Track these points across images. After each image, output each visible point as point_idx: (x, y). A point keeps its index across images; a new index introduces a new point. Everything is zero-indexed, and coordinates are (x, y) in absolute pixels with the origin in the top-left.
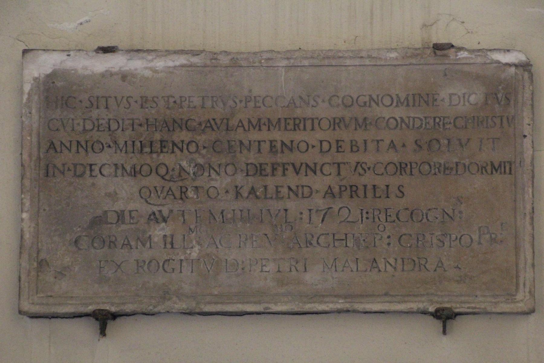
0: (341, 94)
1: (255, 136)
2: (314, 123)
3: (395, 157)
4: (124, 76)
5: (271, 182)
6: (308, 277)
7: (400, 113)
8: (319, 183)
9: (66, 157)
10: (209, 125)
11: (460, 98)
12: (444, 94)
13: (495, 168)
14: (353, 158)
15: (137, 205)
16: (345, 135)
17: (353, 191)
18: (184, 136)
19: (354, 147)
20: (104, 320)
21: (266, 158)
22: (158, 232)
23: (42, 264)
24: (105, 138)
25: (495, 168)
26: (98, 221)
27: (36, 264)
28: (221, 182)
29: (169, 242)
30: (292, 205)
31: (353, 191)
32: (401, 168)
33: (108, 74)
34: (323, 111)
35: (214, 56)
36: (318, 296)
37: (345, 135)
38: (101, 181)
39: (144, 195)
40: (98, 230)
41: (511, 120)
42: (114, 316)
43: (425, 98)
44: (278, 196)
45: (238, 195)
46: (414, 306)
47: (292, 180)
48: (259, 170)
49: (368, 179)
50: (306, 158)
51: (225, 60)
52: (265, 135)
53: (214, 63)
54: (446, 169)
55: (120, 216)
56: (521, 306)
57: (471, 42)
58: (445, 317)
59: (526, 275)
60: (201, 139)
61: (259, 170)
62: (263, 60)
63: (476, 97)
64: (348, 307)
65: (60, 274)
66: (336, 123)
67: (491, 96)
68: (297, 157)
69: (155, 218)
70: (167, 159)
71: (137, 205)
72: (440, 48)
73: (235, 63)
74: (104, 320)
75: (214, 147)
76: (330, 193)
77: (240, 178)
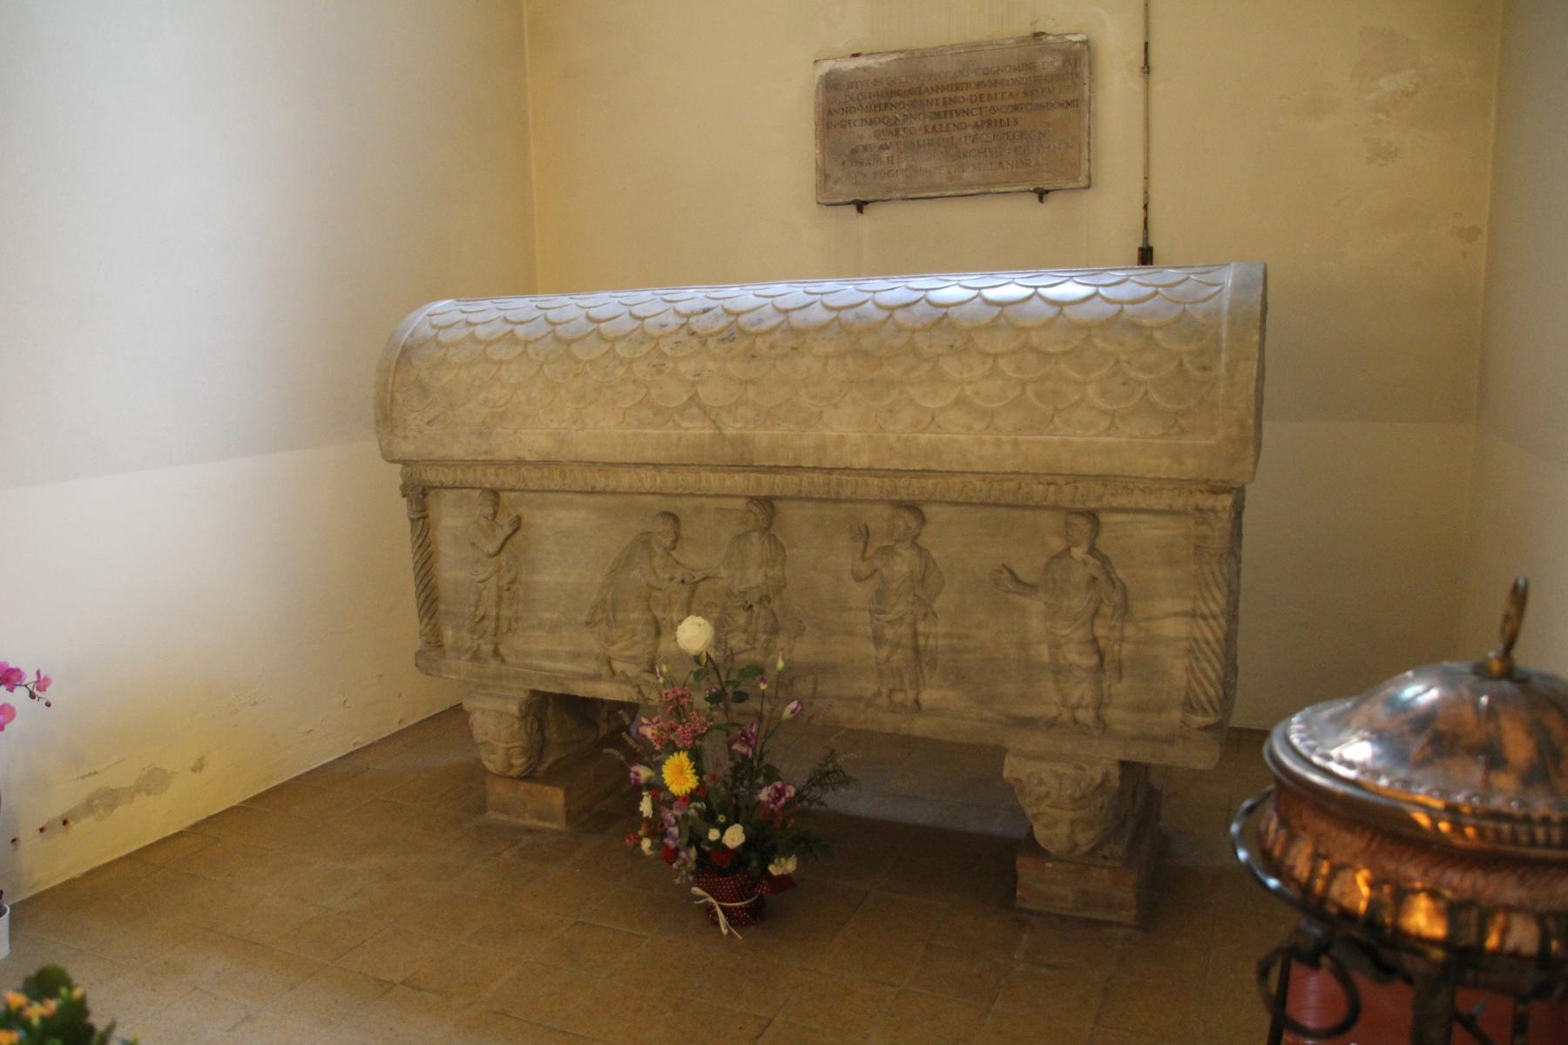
1: (935, 96)
3: (1012, 102)
4: (865, 69)
5: (944, 122)
6: (965, 175)
7: (1014, 75)
8: (970, 120)
9: (836, 118)
10: (911, 92)
11: (1049, 64)
12: (1039, 62)
14: (988, 104)
15: (873, 141)
16: (985, 91)
17: (989, 123)
18: (898, 99)
19: (990, 98)
20: (860, 206)
21: (941, 108)
22: (885, 155)
24: (856, 105)
26: (854, 151)
27: (824, 177)
28: (917, 124)
29: (890, 160)
30: (956, 134)
31: (989, 123)
32: (1016, 108)
33: (857, 69)
34: (973, 78)
35: (912, 52)
36: (970, 185)
37: (985, 91)
38: (854, 129)
39: (877, 135)
41: (1077, 75)
42: (866, 203)
43: (1029, 66)
44: (948, 130)
45: (926, 131)
46: (1022, 188)
47: (956, 120)
48: (938, 115)
49: (997, 116)
50: (963, 106)
51: (917, 54)
52: (940, 95)
53: (913, 57)
54: (1041, 107)
55: (865, 148)
56: (1082, 184)
57: (1058, 31)
58: (1042, 194)
59: (1085, 166)
60: (906, 100)
61: (938, 115)
62: (939, 52)
64: (983, 191)
65: (836, 182)
66: (979, 84)
67: (1066, 61)
68: (958, 106)
69: (883, 147)
70: (888, 113)
71: (873, 141)
72: (1037, 35)
73: (924, 54)
74: (860, 206)
75: (913, 104)
76: (977, 126)
77: (927, 121)
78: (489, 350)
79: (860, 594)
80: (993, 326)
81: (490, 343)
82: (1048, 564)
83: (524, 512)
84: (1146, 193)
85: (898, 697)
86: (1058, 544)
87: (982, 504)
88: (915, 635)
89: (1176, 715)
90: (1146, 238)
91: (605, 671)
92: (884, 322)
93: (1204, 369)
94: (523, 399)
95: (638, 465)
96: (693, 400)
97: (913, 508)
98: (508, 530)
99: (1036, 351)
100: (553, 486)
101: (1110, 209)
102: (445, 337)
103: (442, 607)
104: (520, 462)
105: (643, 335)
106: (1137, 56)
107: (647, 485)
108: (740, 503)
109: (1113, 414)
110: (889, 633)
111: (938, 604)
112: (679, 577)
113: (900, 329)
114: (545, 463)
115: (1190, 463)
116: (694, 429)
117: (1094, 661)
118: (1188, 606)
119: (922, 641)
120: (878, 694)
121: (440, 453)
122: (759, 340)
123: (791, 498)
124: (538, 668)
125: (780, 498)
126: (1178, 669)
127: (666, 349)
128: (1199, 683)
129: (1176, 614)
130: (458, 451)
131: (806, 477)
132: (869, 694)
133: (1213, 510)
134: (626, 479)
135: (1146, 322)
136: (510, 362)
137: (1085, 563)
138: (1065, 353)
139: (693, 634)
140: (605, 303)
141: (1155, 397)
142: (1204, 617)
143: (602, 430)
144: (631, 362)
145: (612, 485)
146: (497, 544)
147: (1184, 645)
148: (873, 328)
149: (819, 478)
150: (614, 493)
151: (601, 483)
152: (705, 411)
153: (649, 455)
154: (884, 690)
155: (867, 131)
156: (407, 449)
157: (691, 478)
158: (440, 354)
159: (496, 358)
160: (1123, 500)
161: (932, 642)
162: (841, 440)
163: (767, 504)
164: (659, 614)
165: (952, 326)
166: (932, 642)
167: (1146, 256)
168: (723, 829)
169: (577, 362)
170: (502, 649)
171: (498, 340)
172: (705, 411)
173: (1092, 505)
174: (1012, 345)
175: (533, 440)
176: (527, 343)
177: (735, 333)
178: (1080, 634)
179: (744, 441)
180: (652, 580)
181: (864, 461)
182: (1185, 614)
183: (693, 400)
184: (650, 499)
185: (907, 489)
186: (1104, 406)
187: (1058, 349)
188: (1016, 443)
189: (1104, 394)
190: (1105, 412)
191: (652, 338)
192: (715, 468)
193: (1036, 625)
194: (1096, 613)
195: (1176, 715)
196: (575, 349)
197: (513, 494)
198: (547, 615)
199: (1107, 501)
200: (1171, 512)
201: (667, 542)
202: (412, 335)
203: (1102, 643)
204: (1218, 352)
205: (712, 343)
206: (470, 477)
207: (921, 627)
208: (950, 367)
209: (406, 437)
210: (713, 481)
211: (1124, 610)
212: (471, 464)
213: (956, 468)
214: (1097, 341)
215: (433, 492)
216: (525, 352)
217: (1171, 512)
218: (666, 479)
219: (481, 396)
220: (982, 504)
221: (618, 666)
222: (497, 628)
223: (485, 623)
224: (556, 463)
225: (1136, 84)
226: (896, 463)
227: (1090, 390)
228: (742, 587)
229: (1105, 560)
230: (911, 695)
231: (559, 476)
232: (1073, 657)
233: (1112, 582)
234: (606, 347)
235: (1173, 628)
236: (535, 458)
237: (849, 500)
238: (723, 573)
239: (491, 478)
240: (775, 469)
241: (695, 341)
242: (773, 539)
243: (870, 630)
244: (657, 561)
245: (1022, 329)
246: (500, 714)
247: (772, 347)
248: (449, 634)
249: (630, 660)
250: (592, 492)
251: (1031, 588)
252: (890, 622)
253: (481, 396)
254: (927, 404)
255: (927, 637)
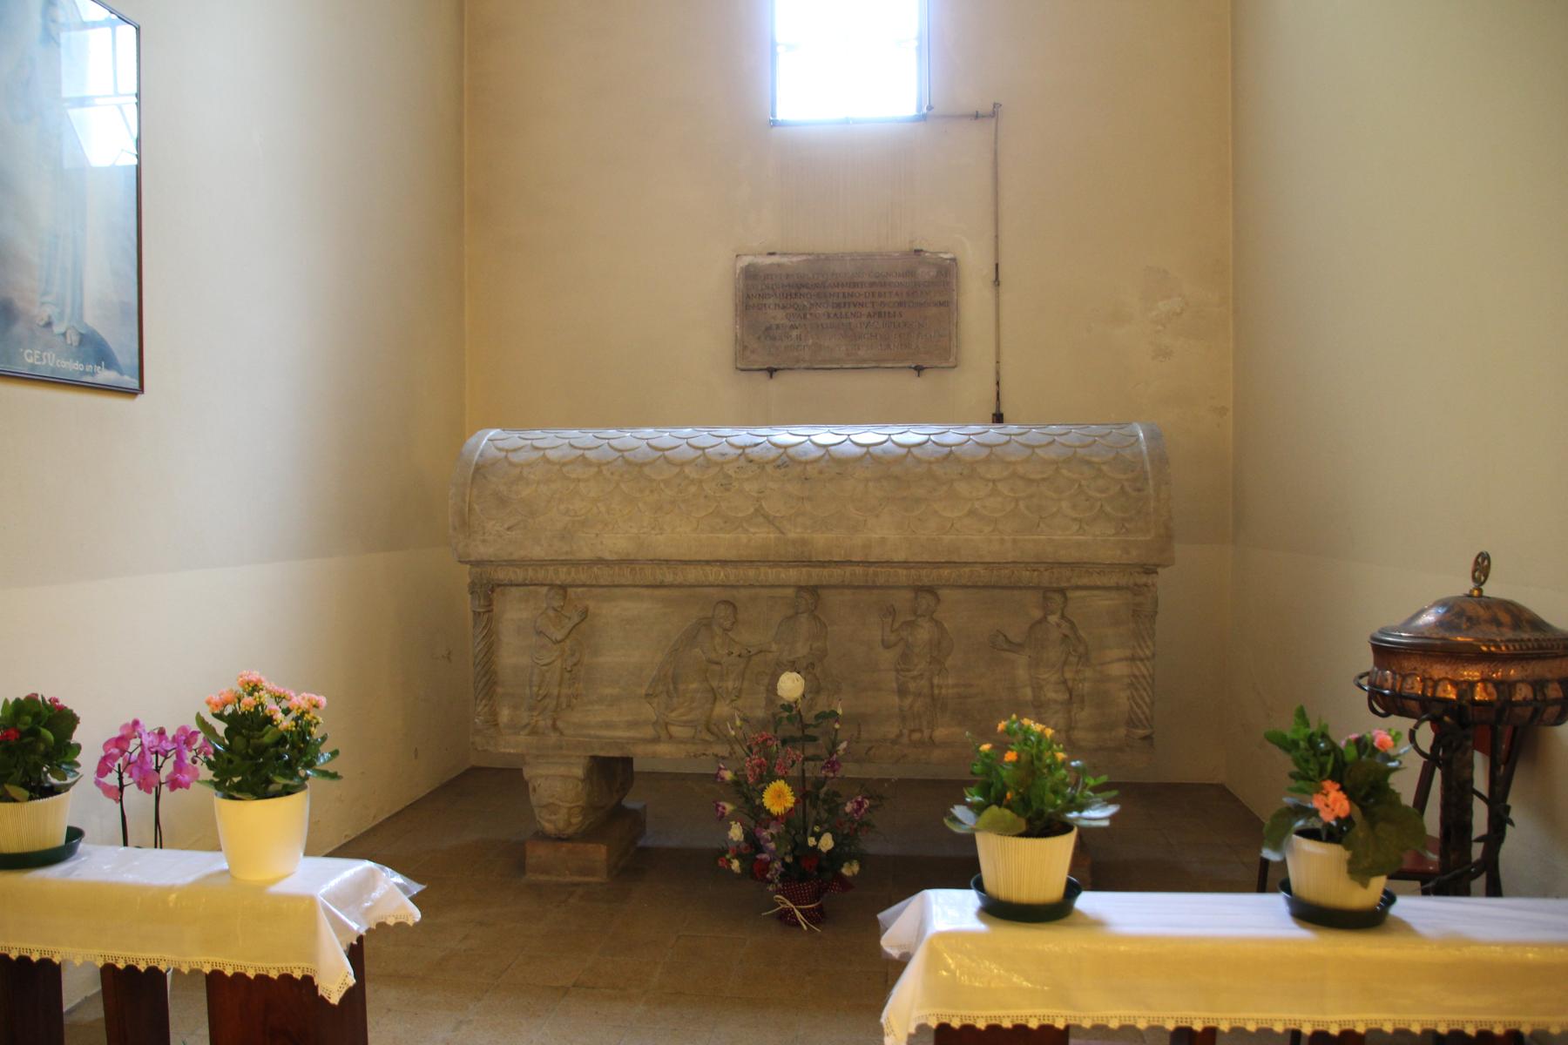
0: (170, 734)
2: (863, 284)
3: (896, 299)
4: (779, 265)
5: (843, 311)
7: (900, 280)
8: (865, 311)
10: (816, 286)
11: (926, 273)
12: (920, 271)
13: (941, 304)
15: (785, 321)
17: (880, 314)
19: (880, 295)
22: (795, 333)
23: (745, 348)
25: (941, 304)
26: (768, 329)
27: (742, 348)
28: (821, 311)
29: (799, 338)
30: (853, 320)
31: (880, 314)
33: (772, 265)
36: (865, 361)
40: (768, 332)
43: (910, 273)
47: (853, 309)
48: (838, 305)
49: (886, 309)
58: (919, 369)
61: (838, 305)
63: (933, 273)
64: (878, 366)
65: (753, 352)
66: (872, 284)
68: (854, 300)
69: (793, 327)
70: (798, 301)
71: (785, 321)
72: (918, 252)
74: (771, 371)
75: (818, 295)
76: (869, 315)
78: (565, 469)
79: (888, 657)
80: (987, 461)
81: (565, 464)
82: (1032, 627)
83: (591, 604)
84: (998, 373)
85: (916, 736)
86: (1037, 614)
87: (985, 587)
88: (932, 686)
89: (1122, 731)
90: (998, 407)
91: (663, 734)
92: (905, 456)
93: (1139, 490)
94: (603, 509)
95: (708, 562)
96: (759, 511)
97: (931, 590)
98: (576, 619)
99: (1022, 478)
100: (623, 581)
101: (972, 383)
102: (514, 458)
103: (500, 690)
104: (600, 561)
105: (706, 461)
106: (989, 271)
107: (711, 578)
108: (790, 592)
109: (1080, 521)
110: (912, 686)
111: (949, 662)
112: (736, 651)
113: (919, 461)
114: (626, 562)
115: (1134, 553)
116: (760, 536)
117: (1067, 696)
118: (1128, 653)
119: (936, 691)
120: (901, 735)
121: (518, 554)
122: (809, 467)
123: (834, 587)
124: (598, 737)
125: (823, 587)
126: (1122, 698)
127: (731, 472)
128: (1139, 707)
129: (1120, 660)
130: (538, 552)
131: (849, 570)
132: (892, 736)
133: (1146, 585)
134: (692, 574)
135: (1095, 459)
136: (587, 480)
137: (1059, 625)
138: (1044, 480)
139: (791, 685)
140: (665, 437)
141: (1108, 509)
142: (1141, 660)
143: (679, 535)
144: (701, 481)
145: (679, 579)
146: (565, 631)
147: (1127, 681)
148: (899, 460)
149: (859, 570)
150: (680, 586)
151: (669, 578)
152: (770, 520)
153: (722, 554)
154: (906, 732)
155: (780, 314)
156: (482, 551)
157: (751, 573)
158: (517, 471)
159: (573, 476)
160: (1085, 581)
161: (944, 691)
162: (883, 540)
163: (814, 590)
164: (715, 684)
165: (958, 460)
166: (944, 691)
167: (998, 418)
168: (818, 837)
169: (651, 480)
170: (560, 724)
171: (572, 462)
172: (770, 520)
173: (1064, 585)
174: (1005, 474)
175: (615, 543)
176: (599, 465)
177: (785, 460)
178: (1055, 677)
179: (804, 542)
180: (713, 656)
181: (900, 556)
182: (1126, 659)
183: (759, 511)
184: (711, 590)
185: (927, 577)
186: (1074, 515)
187: (1039, 476)
188: (1015, 541)
189: (1074, 507)
190: (1075, 519)
191: (716, 464)
192: (776, 564)
193: (1022, 673)
194: (1065, 663)
195: (1122, 731)
196: (647, 470)
197: (580, 590)
198: (608, 691)
199: (1074, 581)
200: (1118, 588)
201: (727, 624)
202: (481, 455)
203: (1070, 684)
204: (1146, 479)
205: (769, 469)
206: (541, 575)
207: (936, 681)
208: (962, 488)
209: (484, 541)
210: (770, 574)
211: (1085, 659)
212: (541, 563)
213: (971, 560)
214: (1064, 472)
215: (498, 590)
216: (600, 472)
217: (1118, 588)
218: (732, 574)
219: (562, 507)
220: (985, 587)
221: (674, 730)
222: (558, 705)
223: (547, 700)
224: (632, 562)
225: (988, 294)
226: (926, 558)
227: (1064, 504)
228: (791, 658)
229: (1072, 626)
230: (927, 733)
231: (635, 573)
232: (1051, 695)
233: (1079, 638)
234: (677, 470)
235: (1118, 669)
236: (615, 557)
237: (881, 587)
238: (774, 647)
239: (563, 576)
240: (823, 564)
241: (755, 467)
242: (816, 618)
243: (895, 685)
244: (718, 640)
245: (1010, 463)
246: (564, 777)
247: (821, 472)
248: (505, 715)
249: (685, 724)
250: (661, 586)
251: (1017, 647)
252: (914, 678)
253: (562, 507)
254: (948, 514)
255: (940, 687)
